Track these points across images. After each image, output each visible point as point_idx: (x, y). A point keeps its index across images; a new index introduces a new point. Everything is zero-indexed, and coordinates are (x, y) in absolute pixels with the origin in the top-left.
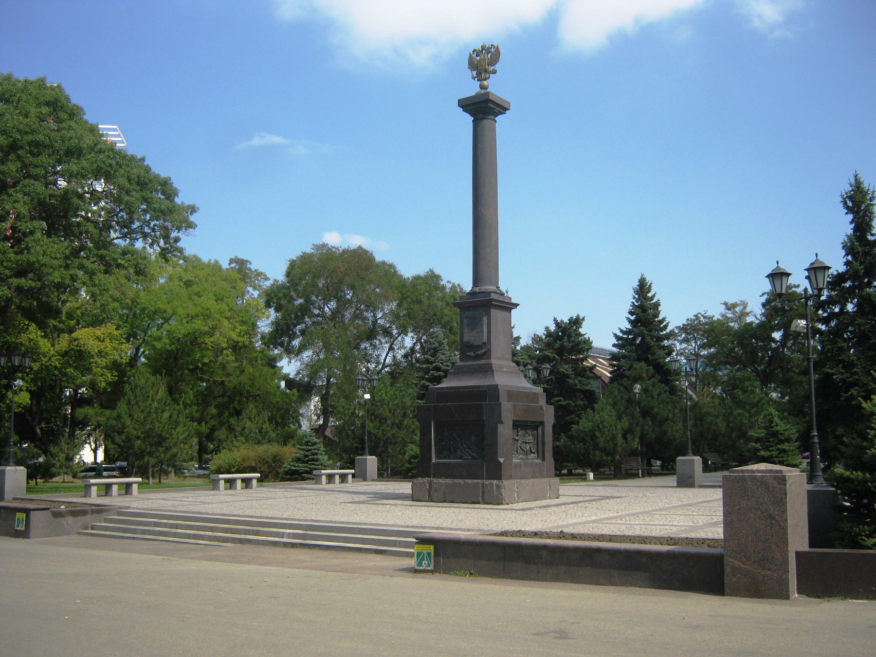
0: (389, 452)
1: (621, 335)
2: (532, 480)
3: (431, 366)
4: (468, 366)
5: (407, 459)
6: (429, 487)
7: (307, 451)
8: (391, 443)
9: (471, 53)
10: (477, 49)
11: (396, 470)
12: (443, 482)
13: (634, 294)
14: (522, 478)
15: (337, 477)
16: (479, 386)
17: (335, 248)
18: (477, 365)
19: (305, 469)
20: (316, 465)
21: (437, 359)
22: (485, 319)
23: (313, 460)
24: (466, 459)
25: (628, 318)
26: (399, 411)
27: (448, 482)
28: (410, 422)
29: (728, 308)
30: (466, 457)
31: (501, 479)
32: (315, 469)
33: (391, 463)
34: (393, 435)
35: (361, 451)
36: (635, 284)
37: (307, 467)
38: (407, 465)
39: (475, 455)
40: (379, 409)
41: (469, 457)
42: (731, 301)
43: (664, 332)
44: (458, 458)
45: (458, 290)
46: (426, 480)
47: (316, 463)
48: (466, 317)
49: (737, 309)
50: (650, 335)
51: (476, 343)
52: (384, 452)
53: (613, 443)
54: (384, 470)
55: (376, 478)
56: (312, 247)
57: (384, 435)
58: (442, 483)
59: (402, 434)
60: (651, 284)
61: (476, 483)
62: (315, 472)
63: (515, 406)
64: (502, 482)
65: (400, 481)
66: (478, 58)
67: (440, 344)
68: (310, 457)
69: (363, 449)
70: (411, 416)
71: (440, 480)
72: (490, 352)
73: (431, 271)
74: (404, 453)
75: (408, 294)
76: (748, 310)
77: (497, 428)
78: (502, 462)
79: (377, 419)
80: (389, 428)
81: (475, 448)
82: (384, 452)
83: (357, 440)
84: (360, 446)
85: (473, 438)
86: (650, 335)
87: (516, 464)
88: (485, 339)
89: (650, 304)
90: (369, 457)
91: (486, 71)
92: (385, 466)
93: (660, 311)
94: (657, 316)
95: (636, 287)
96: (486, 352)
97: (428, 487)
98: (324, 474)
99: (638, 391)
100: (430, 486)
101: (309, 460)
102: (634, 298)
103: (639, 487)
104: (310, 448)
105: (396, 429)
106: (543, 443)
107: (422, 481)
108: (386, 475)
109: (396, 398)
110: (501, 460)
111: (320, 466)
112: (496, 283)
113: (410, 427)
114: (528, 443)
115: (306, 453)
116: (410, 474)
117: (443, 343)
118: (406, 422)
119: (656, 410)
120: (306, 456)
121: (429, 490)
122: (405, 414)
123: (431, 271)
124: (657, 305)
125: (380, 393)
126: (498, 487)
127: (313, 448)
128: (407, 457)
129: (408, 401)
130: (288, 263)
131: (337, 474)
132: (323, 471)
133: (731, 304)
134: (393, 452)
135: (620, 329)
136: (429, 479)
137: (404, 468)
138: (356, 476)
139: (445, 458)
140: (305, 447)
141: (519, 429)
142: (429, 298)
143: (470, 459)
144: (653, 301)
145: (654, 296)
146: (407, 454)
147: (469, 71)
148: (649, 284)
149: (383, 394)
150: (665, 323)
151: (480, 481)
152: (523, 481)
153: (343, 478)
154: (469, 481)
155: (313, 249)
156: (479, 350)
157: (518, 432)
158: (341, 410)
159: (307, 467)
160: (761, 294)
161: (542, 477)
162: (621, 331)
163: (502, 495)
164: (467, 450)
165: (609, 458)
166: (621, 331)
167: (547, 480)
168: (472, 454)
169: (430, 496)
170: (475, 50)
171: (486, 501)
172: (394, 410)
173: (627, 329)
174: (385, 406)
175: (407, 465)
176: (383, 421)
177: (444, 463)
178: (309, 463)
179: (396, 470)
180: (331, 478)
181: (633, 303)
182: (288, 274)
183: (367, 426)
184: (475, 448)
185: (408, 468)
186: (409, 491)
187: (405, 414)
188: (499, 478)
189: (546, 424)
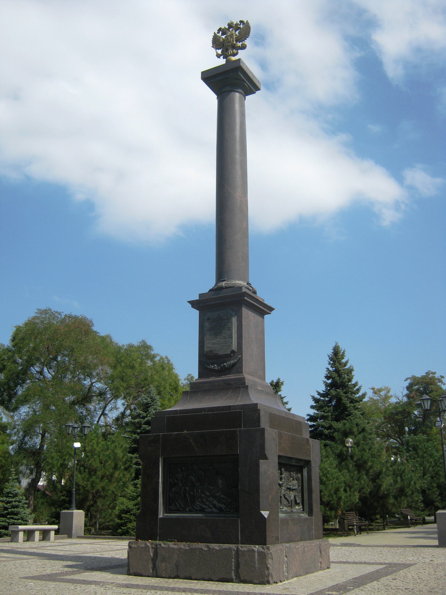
0: (98, 506)
1: (318, 397)
2: (302, 543)
3: (143, 421)
4: (210, 382)
5: (117, 513)
6: (154, 554)
7: (7, 503)
8: (100, 496)
9: (216, 32)
10: (223, 27)
11: (104, 525)
12: (175, 547)
13: (329, 361)
14: (289, 541)
15: (37, 534)
16: (229, 407)
17: (57, 312)
18: (223, 381)
19: (3, 524)
20: (15, 519)
21: (149, 414)
22: (234, 320)
23: (16, 514)
24: (209, 513)
25: (325, 382)
26: (110, 462)
27: (182, 547)
28: (121, 475)
29: (375, 393)
30: (209, 510)
31: (265, 544)
32: (14, 524)
33: (99, 518)
34: (103, 489)
35: (67, 504)
36: (330, 352)
37: (5, 521)
38: (117, 521)
39: (223, 506)
40: (89, 460)
41: (214, 510)
42: (377, 387)
43: (357, 396)
44: (197, 511)
45: (166, 362)
46: (149, 543)
47: (16, 517)
48: (208, 319)
49: (382, 393)
50: (346, 397)
51: (221, 353)
52: (92, 506)
53: (336, 497)
54: (91, 526)
55: (83, 535)
56: (37, 311)
57: (93, 487)
58: (173, 549)
59: (112, 487)
60: (344, 351)
61: (226, 549)
62: (11, 528)
63: (280, 436)
64: (268, 548)
65: (109, 538)
66: (224, 37)
67: (153, 399)
68: (10, 510)
69: (70, 502)
70: (122, 468)
71: (170, 543)
72: (242, 363)
73: (144, 341)
74: (114, 508)
75: (122, 359)
76: (390, 394)
77: (258, 466)
78: (266, 516)
79: (87, 470)
80: (98, 480)
81: (222, 496)
82: (92, 506)
83: (64, 493)
84: (68, 499)
85: (220, 482)
86: (346, 397)
87: (282, 520)
88: (234, 347)
89: (344, 370)
90: (76, 511)
91: (234, 47)
92: (94, 520)
93: (353, 376)
94: (350, 380)
95: (331, 354)
96: (236, 363)
97: (152, 554)
98: (21, 530)
99: (350, 445)
100: (156, 553)
101: (8, 514)
102: (329, 364)
103: (370, 546)
104: (10, 500)
105: (106, 481)
106: (310, 491)
107: (143, 545)
108: (93, 530)
109: (108, 449)
110: (265, 514)
111: (20, 521)
112: (245, 278)
113: (121, 479)
114: (293, 490)
115: (5, 505)
116: (120, 531)
117: (155, 399)
118: (116, 475)
119: (370, 464)
120: (6, 509)
121: (154, 560)
122: (116, 465)
123: (144, 341)
124: (350, 371)
125: (91, 443)
126: (263, 556)
127: (13, 500)
128: (116, 512)
129: (120, 453)
130: (14, 329)
131: (37, 530)
132: (21, 527)
133: (377, 389)
134: (102, 506)
135: (317, 392)
136: (154, 542)
137: (112, 523)
138: (61, 531)
139: (178, 511)
140: (4, 499)
141: (283, 469)
142: (141, 364)
143: (217, 513)
144: (347, 367)
145: (347, 362)
146: (117, 508)
147: (214, 50)
148: (342, 351)
149: (94, 444)
150: (357, 387)
151: (233, 546)
152: (292, 545)
153: (45, 534)
154: (216, 546)
155: (37, 313)
156: (226, 362)
157: (281, 474)
158: (50, 461)
159: (5, 521)
160: (405, 379)
161: (311, 538)
162: (319, 394)
163: (268, 568)
164: (211, 499)
165: (333, 513)
166: (319, 394)
167: (316, 542)
168: (218, 505)
169: (154, 567)
170: (220, 29)
171: (242, 579)
172: (105, 461)
173: (324, 392)
174: (95, 457)
175: (117, 521)
176: (93, 473)
177: (177, 519)
178: (8, 516)
179: (104, 525)
180: (29, 535)
181: (328, 369)
182: (14, 339)
183: (75, 478)
184: (222, 496)
185: (118, 524)
186: (123, 555)
187: (116, 465)
188: (263, 542)
189: (313, 464)
